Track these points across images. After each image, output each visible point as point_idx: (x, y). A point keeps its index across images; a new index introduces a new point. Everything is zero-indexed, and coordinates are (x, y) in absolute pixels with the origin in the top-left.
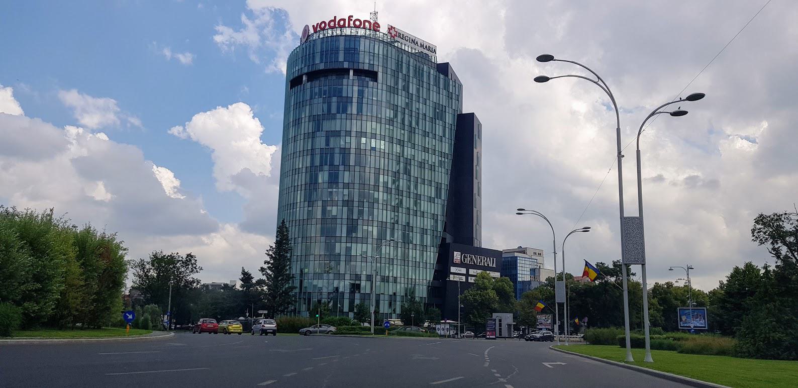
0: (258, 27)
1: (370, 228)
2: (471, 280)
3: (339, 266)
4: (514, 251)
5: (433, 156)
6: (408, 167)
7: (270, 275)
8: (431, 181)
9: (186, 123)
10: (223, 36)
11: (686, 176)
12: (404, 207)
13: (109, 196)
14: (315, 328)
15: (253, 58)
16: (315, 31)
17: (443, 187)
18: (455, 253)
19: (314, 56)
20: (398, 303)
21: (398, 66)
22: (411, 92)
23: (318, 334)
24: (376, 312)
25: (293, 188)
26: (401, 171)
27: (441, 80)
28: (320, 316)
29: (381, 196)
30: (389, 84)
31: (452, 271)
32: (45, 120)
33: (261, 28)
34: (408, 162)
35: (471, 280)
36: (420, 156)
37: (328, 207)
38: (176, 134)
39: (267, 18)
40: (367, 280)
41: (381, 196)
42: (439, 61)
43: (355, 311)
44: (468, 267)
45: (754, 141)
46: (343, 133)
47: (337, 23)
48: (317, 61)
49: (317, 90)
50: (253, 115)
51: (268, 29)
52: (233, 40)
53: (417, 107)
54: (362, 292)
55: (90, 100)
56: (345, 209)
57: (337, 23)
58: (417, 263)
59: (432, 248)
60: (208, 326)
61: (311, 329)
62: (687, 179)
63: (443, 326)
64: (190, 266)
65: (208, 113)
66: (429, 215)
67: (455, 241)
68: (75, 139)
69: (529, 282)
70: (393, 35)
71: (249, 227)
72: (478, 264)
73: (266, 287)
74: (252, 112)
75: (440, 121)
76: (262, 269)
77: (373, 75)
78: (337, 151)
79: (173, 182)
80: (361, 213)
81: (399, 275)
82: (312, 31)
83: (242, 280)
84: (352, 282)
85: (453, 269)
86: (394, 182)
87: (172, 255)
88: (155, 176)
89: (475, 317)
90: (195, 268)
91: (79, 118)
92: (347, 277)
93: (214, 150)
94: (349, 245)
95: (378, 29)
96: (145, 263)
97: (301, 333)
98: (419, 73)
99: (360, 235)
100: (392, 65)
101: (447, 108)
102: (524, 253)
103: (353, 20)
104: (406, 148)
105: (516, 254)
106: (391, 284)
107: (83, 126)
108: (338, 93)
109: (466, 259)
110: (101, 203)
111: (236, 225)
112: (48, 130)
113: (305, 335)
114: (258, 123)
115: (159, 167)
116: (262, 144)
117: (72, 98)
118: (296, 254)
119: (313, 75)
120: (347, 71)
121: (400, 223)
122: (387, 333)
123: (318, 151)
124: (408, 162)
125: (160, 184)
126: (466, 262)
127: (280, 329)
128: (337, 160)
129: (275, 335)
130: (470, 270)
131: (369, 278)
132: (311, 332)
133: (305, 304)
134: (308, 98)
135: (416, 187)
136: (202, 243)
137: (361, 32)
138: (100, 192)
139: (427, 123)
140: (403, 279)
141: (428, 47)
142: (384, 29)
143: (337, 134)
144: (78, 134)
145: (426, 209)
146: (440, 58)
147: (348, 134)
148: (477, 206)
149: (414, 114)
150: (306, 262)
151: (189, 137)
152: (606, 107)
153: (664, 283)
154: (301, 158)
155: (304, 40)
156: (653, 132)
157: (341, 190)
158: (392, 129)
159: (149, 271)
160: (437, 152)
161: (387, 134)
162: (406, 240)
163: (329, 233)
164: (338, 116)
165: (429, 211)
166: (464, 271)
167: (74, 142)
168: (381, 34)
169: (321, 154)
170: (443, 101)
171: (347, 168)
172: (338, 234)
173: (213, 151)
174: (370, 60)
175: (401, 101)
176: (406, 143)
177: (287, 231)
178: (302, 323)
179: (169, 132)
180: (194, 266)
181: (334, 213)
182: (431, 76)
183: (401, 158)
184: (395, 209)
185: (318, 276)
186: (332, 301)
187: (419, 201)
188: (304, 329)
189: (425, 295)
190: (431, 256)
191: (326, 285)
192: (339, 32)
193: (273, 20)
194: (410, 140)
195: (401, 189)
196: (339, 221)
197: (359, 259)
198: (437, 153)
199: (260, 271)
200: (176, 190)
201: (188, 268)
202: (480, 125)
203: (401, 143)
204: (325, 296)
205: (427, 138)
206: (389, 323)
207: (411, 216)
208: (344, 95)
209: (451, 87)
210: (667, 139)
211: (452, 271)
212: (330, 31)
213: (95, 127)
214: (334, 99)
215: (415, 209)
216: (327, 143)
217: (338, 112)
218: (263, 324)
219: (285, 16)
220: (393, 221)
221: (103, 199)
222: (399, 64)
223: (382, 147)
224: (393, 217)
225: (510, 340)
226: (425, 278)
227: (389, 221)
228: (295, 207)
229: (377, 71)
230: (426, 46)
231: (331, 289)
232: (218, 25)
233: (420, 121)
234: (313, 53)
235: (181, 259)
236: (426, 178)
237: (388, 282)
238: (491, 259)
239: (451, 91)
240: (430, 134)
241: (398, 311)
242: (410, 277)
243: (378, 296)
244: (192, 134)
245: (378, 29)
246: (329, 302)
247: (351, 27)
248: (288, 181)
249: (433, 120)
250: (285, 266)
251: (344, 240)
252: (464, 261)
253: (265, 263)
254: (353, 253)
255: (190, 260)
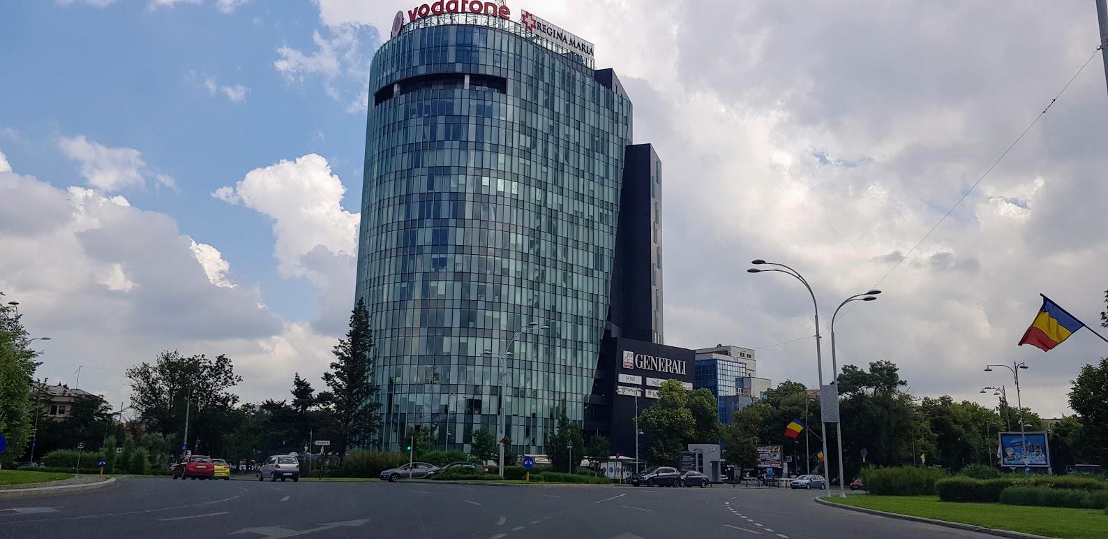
0: (336, 50)
1: (496, 315)
2: (650, 393)
3: (448, 373)
4: (711, 351)
5: (591, 206)
6: (554, 222)
7: (340, 386)
8: (588, 244)
9: (238, 182)
10: (288, 62)
11: (935, 253)
12: (547, 282)
13: (129, 285)
14: (406, 469)
15: (332, 92)
16: (413, 20)
17: (606, 253)
18: (625, 353)
19: (410, 56)
20: (540, 430)
21: (537, 71)
22: (556, 110)
23: (410, 479)
24: (507, 442)
25: (378, 253)
26: (543, 229)
27: (602, 95)
28: (414, 448)
29: (514, 266)
30: (523, 97)
31: (620, 381)
32: (41, 178)
33: (340, 51)
34: (553, 215)
35: (651, 394)
36: (571, 206)
37: (432, 282)
38: (223, 197)
39: (349, 37)
40: (492, 394)
41: (514, 266)
42: (599, 66)
43: (474, 441)
44: (645, 374)
45: (1024, 206)
46: (454, 170)
47: (445, 7)
48: (416, 62)
49: (415, 106)
50: (330, 171)
51: (350, 52)
52: (301, 67)
53: (567, 133)
54: (484, 412)
55: (103, 150)
56: (458, 285)
57: (445, 7)
58: (568, 369)
59: (590, 345)
60: (198, 467)
61: (399, 471)
62: (934, 257)
63: (611, 465)
64: (222, 375)
65: (268, 168)
66: (585, 295)
67: (624, 334)
68: (81, 205)
69: (736, 398)
70: (529, 25)
71: (321, 328)
72: (660, 370)
73: (334, 405)
74: (329, 167)
75: (601, 155)
76: (327, 377)
77: (499, 84)
78: (445, 197)
79: (219, 264)
80: (482, 291)
81: (540, 387)
82: (407, 20)
83: (295, 393)
84: (470, 397)
85: (622, 378)
86: (532, 244)
87: (196, 359)
88: (194, 255)
89: (659, 450)
90: (230, 378)
91: (88, 176)
92: (461, 389)
93: (276, 220)
94: (463, 340)
95: (508, 16)
96: (150, 370)
97: (383, 478)
98: (568, 82)
99: (480, 325)
100: (528, 69)
101: (611, 136)
102: (727, 354)
103: (469, 3)
104: (549, 194)
105: (715, 356)
106: (528, 400)
107: (94, 188)
108: (448, 110)
109: (642, 362)
110: (118, 295)
111: (307, 324)
112: (44, 191)
113: (390, 481)
114: (338, 182)
115: (200, 245)
116: (342, 211)
117: (78, 147)
118: (382, 355)
119: (409, 84)
120: (460, 77)
121: (541, 306)
122: (528, 478)
123: (416, 198)
124: (553, 215)
125: (201, 268)
126: (642, 366)
127: (303, 472)
128: (445, 211)
129: (296, 480)
130: (648, 379)
131: (496, 391)
132: (399, 476)
133: (395, 431)
134: (402, 118)
135: (565, 253)
136: (260, 351)
137: (481, 21)
138: (118, 279)
139: (582, 156)
140: (546, 393)
141: (581, 45)
142: (515, 16)
143: (445, 171)
144: (86, 199)
145: (580, 286)
146: (600, 62)
147: (463, 170)
148: (657, 281)
149: (561, 143)
150: (398, 367)
151: (241, 202)
152: (819, 159)
153: (937, 398)
154: (391, 208)
155: (396, 34)
156: (886, 192)
157: (452, 256)
158: (529, 164)
159: (155, 382)
160: (596, 201)
161: (521, 172)
162: (552, 336)
163: (434, 328)
164: (447, 144)
165: (585, 290)
166: (638, 380)
167: (81, 208)
168: (512, 24)
169: (421, 202)
170: (605, 125)
171: (460, 222)
172: (447, 324)
173: (275, 221)
174: (494, 62)
175: (541, 122)
176: (549, 186)
177: (367, 316)
178: (389, 461)
179: (214, 195)
180: (229, 375)
181: (441, 291)
182: (587, 87)
183: (542, 208)
184: (535, 285)
185: (417, 388)
186: (438, 428)
187: (570, 274)
188: (389, 471)
189: (580, 417)
190: (589, 359)
191: (429, 403)
192: (448, 21)
193: (356, 41)
194: (555, 182)
195: (542, 255)
196: (448, 304)
197: (479, 361)
198: (596, 203)
199: (323, 379)
200: (222, 275)
201: (220, 378)
202: (658, 163)
203: (542, 185)
204: (427, 418)
205: (581, 179)
206: (531, 460)
207: (559, 297)
208: (456, 112)
209: (616, 104)
210: (904, 203)
211: (620, 381)
212: (434, 20)
213: (110, 190)
214: (441, 119)
215: (564, 286)
216: (431, 185)
217: (447, 138)
218: (276, 463)
219: (374, 34)
220: (530, 303)
221: (121, 289)
222: (539, 68)
223: (514, 192)
224: (530, 297)
225: (716, 488)
226: (579, 391)
227: (524, 303)
228: (381, 283)
229: (506, 77)
230: (579, 44)
231: (436, 409)
232: (281, 47)
233: (571, 153)
234: (410, 51)
235: (208, 364)
236: (581, 240)
237: (524, 397)
238: (679, 362)
239: (616, 110)
240: (586, 174)
241: (539, 442)
242: (557, 390)
243: (509, 418)
244: (245, 198)
245: (508, 16)
246: (433, 429)
247: (467, 12)
248: (371, 242)
249: (590, 153)
250: (364, 371)
251: (456, 331)
252: (639, 365)
253: (331, 367)
254: (470, 353)
255: (223, 366)
